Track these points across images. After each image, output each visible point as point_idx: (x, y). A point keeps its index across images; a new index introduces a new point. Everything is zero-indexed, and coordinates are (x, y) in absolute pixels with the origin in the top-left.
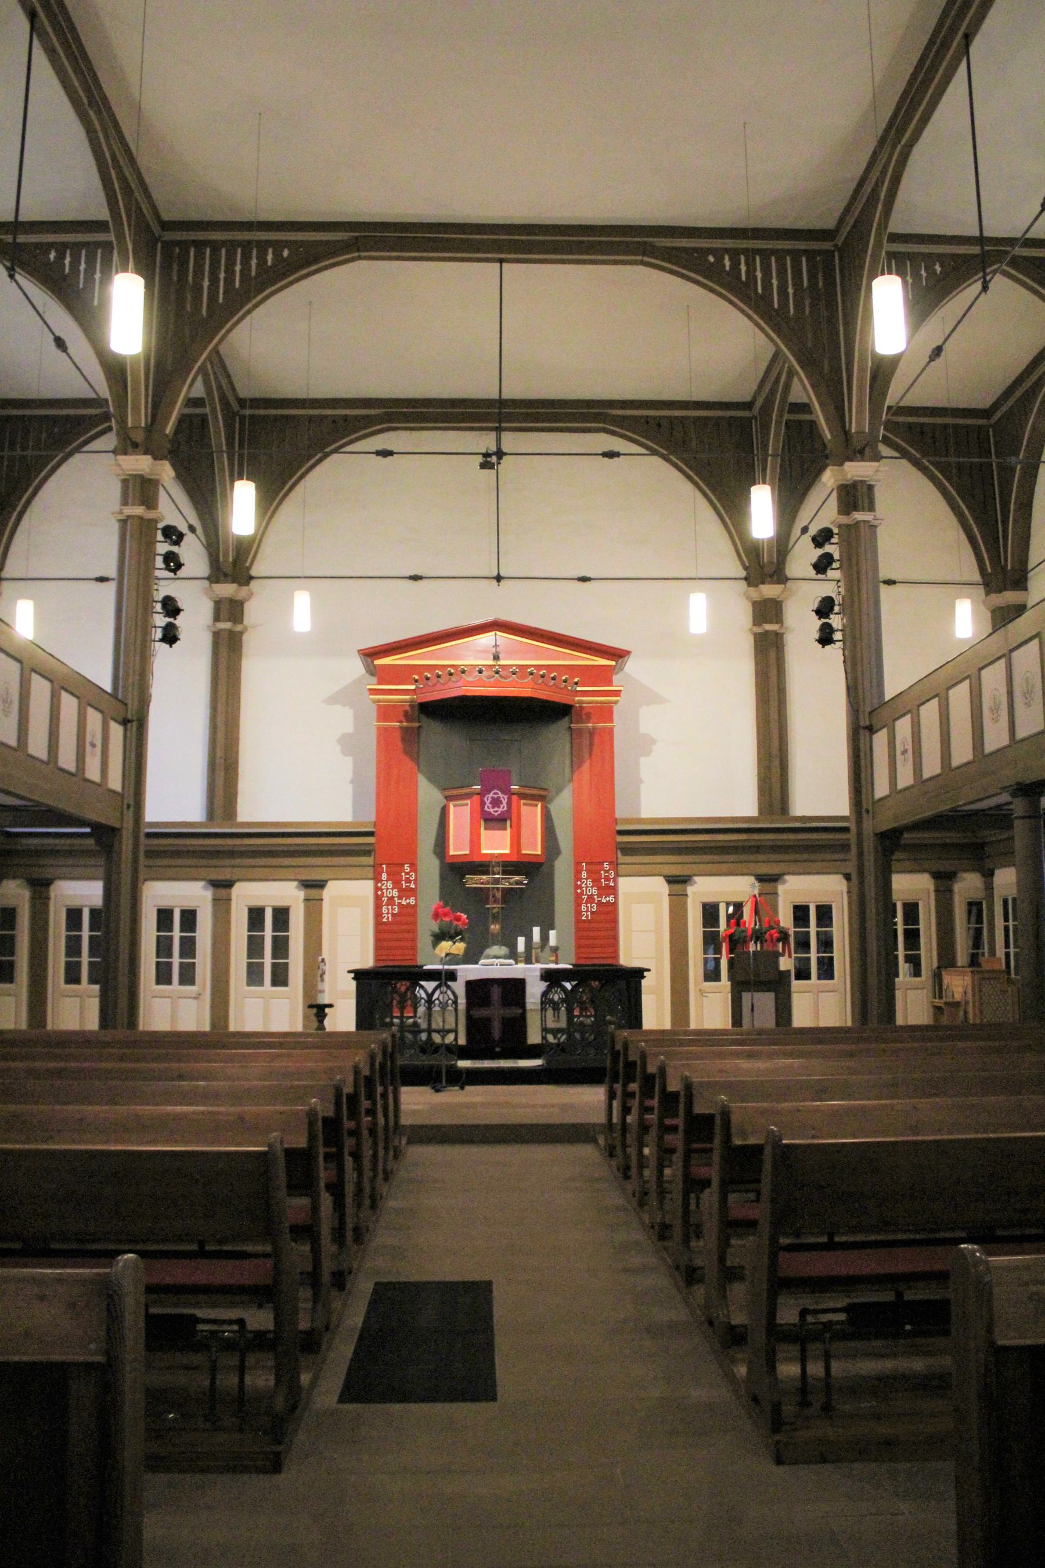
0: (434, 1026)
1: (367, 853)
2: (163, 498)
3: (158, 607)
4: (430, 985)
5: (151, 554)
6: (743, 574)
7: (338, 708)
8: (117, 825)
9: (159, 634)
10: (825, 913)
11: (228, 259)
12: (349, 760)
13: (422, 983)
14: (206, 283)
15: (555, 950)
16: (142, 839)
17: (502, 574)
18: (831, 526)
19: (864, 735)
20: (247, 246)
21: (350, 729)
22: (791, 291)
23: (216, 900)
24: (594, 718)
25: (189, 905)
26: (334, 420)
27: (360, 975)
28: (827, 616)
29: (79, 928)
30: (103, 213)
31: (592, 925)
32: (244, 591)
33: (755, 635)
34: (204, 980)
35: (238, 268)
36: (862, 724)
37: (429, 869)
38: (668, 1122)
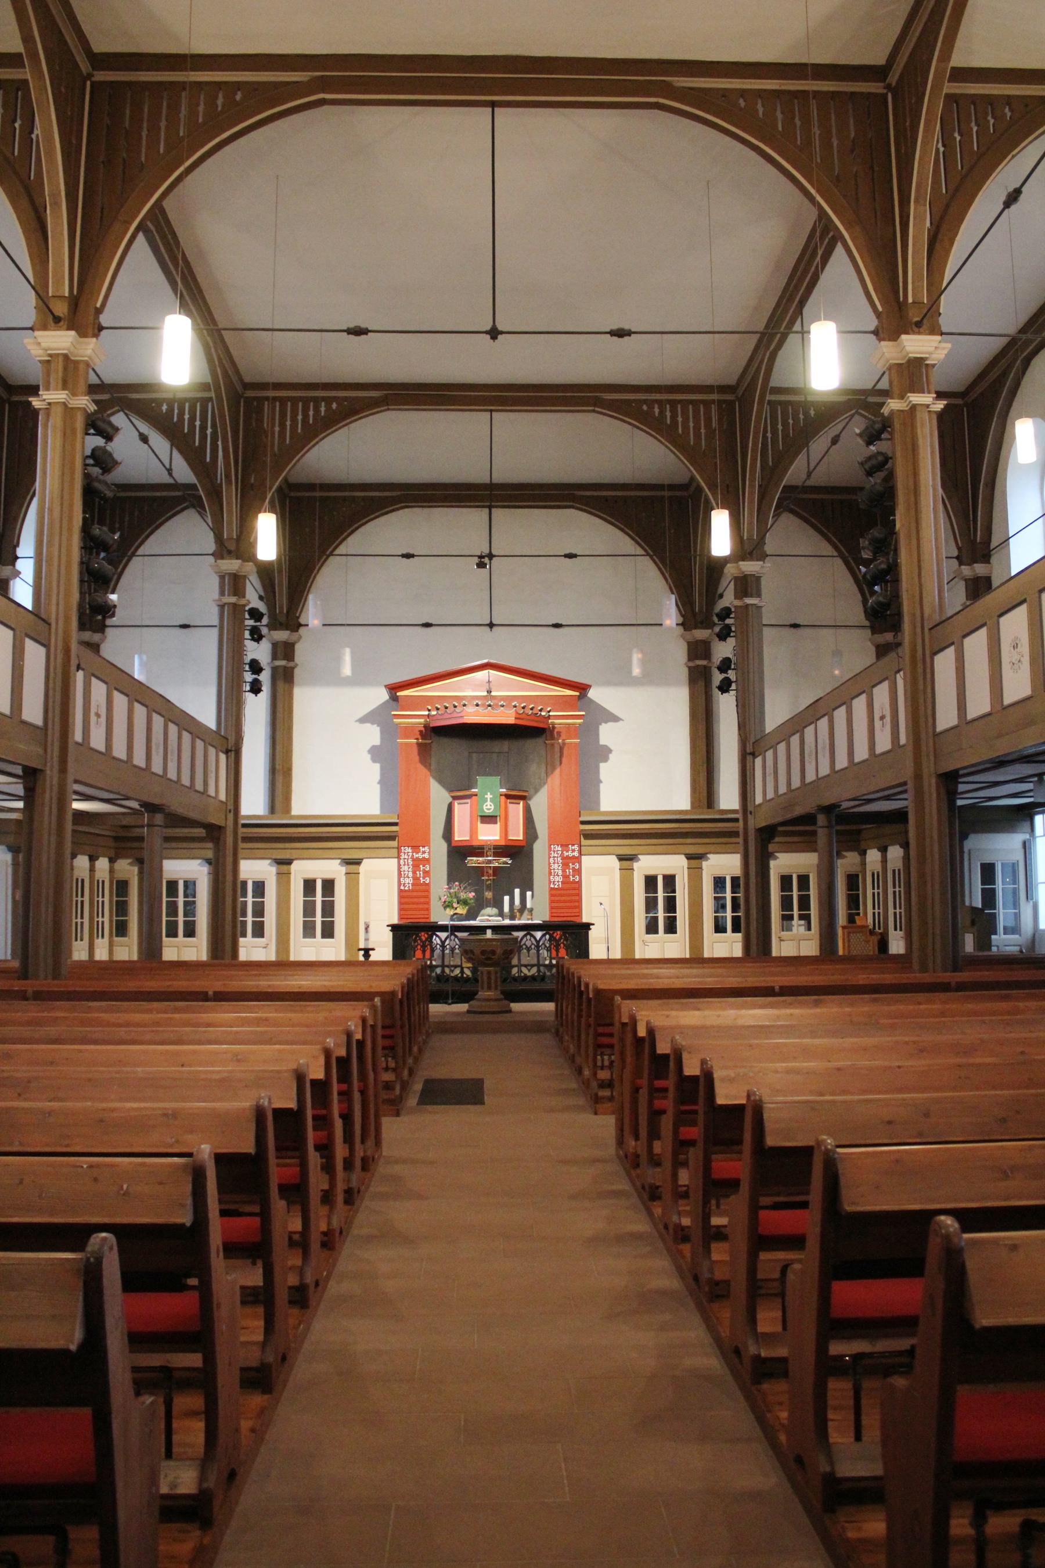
0: (446, 963)
1: (391, 838)
3: (247, 668)
4: (443, 935)
5: (242, 627)
7: (368, 725)
8: (222, 824)
11: (292, 411)
12: (377, 766)
14: (277, 429)
17: (494, 622)
19: (749, 758)
20: (306, 401)
22: (703, 431)
24: (563, 736)
25: (259, 877)
27: (394, 928)
28: (726, 672)
29: (800, 897)
32: (294, 637)
33: (690, 668)
35: (300, 417)
37: (438, 852)
38: (658, 1083)
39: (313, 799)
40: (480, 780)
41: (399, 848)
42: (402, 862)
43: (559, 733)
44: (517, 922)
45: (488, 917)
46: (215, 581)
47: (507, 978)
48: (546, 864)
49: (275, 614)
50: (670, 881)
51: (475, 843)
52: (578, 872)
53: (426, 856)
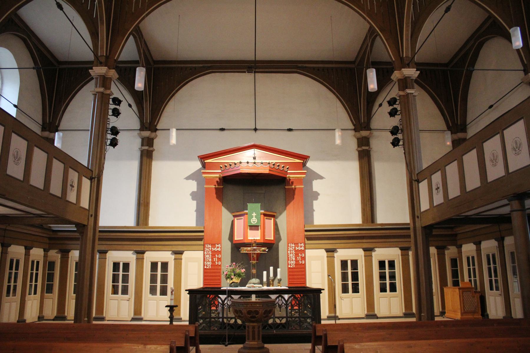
1: (201, 240)
2: (113, 86)
4: (223, 297)
6: (353, 127)
7: (190, 181)
8: (86, 223)
9: (109, 142)
10: (392, 264)
12: (195, 202)
13: (220, 296)
15: (280, 280)
16: (97, 232)
17: (257, 128)
18: (396, 97)
19: (415, 184)
21: (195, 189)
23: (137, 259)
25: (126, 261)
26: (191, 68)
27: (191, 292)
30: (138, 59)
31: (296, 270)
33: (359, 151)
34: (132, 292)
36: (414, 178)
37: (226, 247)
39: (160, 218)
40: (249, 205)
41: (204, 245)
42: (205, 252)
43: (292, 183)
44: (271, 288)
45: (253, 285)
46: (139, 141)
47: (266, 326)
48: (285, 253)
49: (143, 123)
50: (354, 263)
51: (246, 241)
52: (304, 258)
53: (219, 249)
